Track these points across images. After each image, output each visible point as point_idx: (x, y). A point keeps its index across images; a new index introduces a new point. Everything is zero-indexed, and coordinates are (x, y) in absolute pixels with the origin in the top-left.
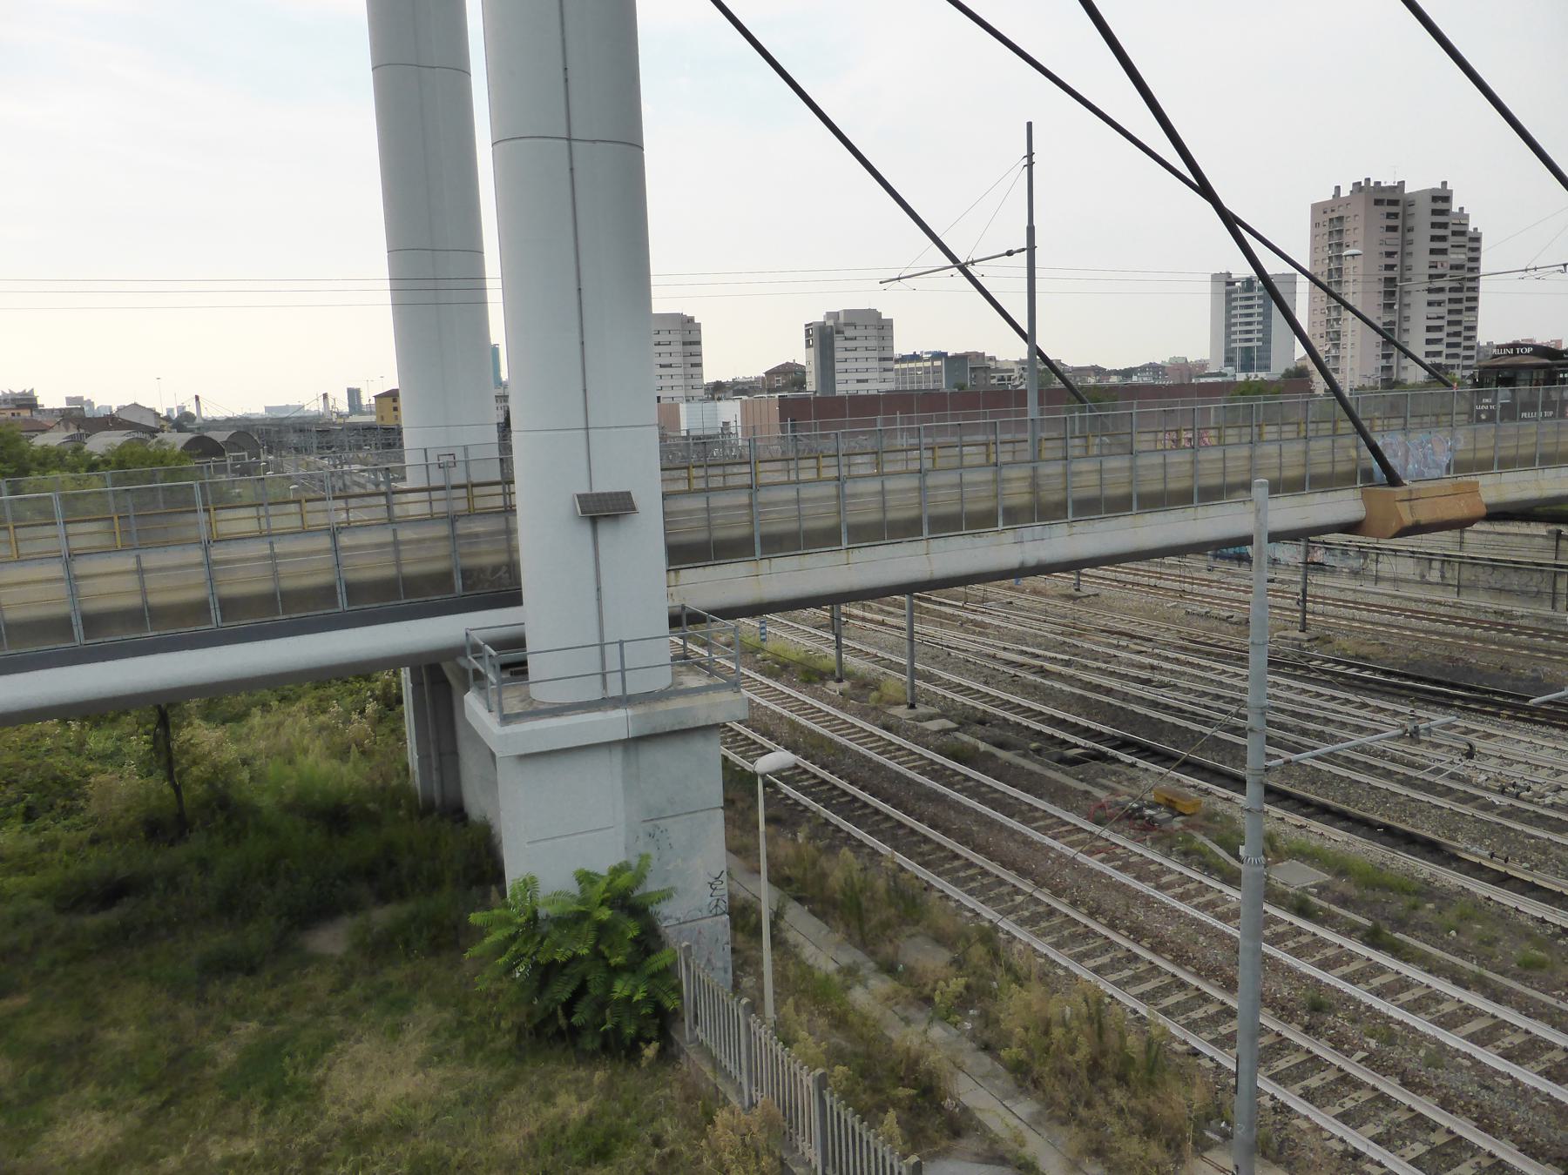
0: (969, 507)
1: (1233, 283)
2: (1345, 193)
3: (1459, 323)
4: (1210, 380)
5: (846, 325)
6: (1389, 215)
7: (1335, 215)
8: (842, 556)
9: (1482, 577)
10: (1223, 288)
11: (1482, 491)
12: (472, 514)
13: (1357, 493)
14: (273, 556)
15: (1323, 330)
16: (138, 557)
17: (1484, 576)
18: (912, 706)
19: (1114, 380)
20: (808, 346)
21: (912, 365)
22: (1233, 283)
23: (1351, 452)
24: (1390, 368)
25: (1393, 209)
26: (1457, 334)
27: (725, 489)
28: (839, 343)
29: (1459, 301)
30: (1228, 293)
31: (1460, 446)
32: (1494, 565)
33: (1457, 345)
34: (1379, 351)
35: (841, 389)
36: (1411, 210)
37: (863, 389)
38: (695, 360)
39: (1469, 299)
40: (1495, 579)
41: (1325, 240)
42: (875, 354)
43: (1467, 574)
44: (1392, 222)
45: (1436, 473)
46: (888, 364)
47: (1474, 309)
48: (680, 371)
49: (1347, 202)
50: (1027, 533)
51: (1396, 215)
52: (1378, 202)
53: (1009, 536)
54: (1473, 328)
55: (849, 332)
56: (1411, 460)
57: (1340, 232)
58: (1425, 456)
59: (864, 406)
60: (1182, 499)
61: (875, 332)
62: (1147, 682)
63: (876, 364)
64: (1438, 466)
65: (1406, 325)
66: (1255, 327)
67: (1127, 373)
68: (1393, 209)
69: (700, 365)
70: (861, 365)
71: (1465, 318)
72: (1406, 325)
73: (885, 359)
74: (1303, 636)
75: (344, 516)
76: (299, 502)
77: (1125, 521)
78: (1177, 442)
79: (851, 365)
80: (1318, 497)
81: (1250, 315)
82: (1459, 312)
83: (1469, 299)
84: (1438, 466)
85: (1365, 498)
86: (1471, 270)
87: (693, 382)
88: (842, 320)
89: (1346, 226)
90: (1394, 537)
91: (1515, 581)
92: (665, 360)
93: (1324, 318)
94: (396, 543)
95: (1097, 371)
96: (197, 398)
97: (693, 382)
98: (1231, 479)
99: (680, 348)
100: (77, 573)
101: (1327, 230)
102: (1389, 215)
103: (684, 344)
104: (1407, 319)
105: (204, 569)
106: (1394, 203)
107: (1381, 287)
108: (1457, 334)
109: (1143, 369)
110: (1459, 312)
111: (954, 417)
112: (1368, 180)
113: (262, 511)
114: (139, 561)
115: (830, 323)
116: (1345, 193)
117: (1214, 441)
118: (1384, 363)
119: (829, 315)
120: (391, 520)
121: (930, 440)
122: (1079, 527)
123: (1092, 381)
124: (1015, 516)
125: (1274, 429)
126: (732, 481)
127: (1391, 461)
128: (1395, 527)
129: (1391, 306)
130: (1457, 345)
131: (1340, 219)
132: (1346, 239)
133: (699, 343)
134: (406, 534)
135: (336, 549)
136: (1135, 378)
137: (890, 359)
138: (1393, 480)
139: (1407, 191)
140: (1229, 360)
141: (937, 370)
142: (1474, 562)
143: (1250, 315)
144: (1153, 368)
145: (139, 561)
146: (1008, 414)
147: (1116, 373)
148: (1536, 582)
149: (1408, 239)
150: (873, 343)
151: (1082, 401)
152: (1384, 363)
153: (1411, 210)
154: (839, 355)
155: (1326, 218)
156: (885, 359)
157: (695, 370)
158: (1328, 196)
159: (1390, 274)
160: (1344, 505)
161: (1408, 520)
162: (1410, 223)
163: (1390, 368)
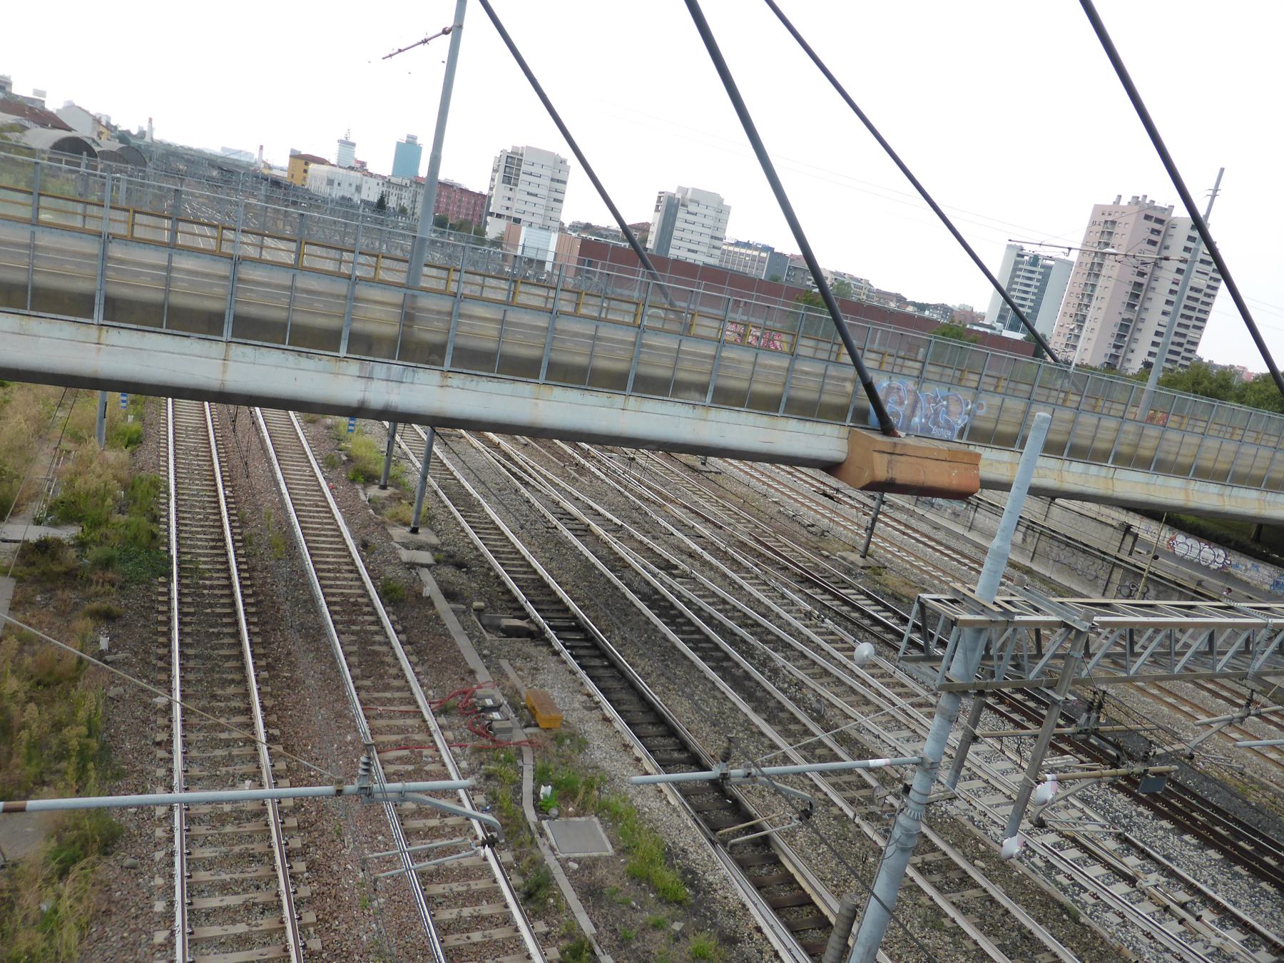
0: (299, 319)
1: (1022, 256)
2: (1124, 202)
3: (1184, 336)
4: (981, 329)
5: (691, 201)
6: (1153, 231)
7: (1110, 218)
8: (93, 331)
9: (1055, 550)
10: (1013, 257)
11: (981, 464)
12: (373, 282)
13: (844, 432)
14: (595, 338)
15: (1073, 311)
16: (33, 233)
17: (1056, 551)
18: (414, 531)
19: (910, 309)
20: (657, 210)
21: (743, 251)
22: (1022, 256)
23: (844, 387)
24: (1117, 357)
25: (1157, 226)
26: (1180, 345)
27: (259, 262)
28: (681, 214)
29: (1190, 318)
30: (1016, 263)
31: (981, 413)
32: (1069, 543)
33: (1178, 354)
34: (1112, 341)
35: (673, 253)
36: (1172, 231)
37: (691, 258)
38: (558, 196)
39: (1197, 319)
40: (1065, 555)
41: (1097, 237)
42: (709, 231)
43: (1044, 544)
44: (1154, 237)
45: (947, 434)
46: (717, 243)
47: (1201, 328)
48: (544, 202)
49: (1123, 211)
50: (380, 370)
51: (1159, 232)
52: (1147, 217)
53: (354, 368)
54: (1196, 344)
55: (692, 208)
56: (918, 412)
57: (1110, 233)
58: (936, 413)
59: (685, 269)
60: (613, 382)
61: (713, 213)
62: (668, 567)
63: (707, 240)
64: (951, 428)
65: (1140, 325)
66: (1030, 296)
67: (922, 307)
68: (1157, 226)
69: (561, 201)
70: (696, 238)
71: (1191, 333)
72: (1140, 325)
73: (716, 238)
74: (861, 562)
75: (477, 289)
76: (448, 270)
77: (524, 388)
78: (743, 336)
79: (686, 235)
80: (793, 424)
81: (1029, 286)
82: (1187, 327)
83: (1197, 319)
84: (951, 428)
85: (851, 439)
86: (1209, 296)
87: (551, 214)
88: (689, 196)
89: (1117, 230)
90: (864, 488)
91: (1081, 562)
92: (533, 190)
93: (1077, 302)
94: (32, 247)
95: (900, 299)
96: (261, 147)
97: (551, 214)
98: (682, 376)
99: (548, 182)
100: (110, 254)
101: (1100, 229)
102: (1153, 231)
103: (552, 180)
104: (1143, 320)
105: (98, 263)
106: (1160, 221)
107: (1130, 289)
108: (1180, 345)
109: (936, 307)
110: (1187, 327)
111: (785, 304)
112: (1145, 197)
113: (552, 294)
114: (170, 261)
115: (679, 196)
116: (1124, 202)
117: (786, 348)
118: (1113, 351)
119: (680, 189)
120: (35, 222)
121: (745, 318)
122: (456, 380)
123: (893, 305)
124: (365, 346)
125: (811, 343)
126: (488, 294)
127: (888, 408)
128: (866, 479)
129: (1134, 306)
130: (1178, 354)
131: (1114, 222)
132: (1113, 241)
133: (565, 182)
134: (304, 282)
135: (105, 257)
136: (927, 313)
137: (721, 239)
138: (886, 428)
139: (1173, 215)
140: (1001, 318)
141: (762, 260)
142: (1053, 535)
143: (1029, 286)
144: (944, 309)
145: (170, 261)
146: (751, 297)
147: (914, 304)
148: (1096, 568)
149: (1170, 254)
150: (708, 222)
151: (647, 267)
152: (1113, 351)
153: (1172, 231)
154: (678, 224)
155: (1103, 219)
156: (716, 238)
157: (556, 205)
158: (1109, 201)
159: (1140, 280)
160: (825, 440)
161: (882, 474)
162: (1168, 242)
163: (1117, 357)
